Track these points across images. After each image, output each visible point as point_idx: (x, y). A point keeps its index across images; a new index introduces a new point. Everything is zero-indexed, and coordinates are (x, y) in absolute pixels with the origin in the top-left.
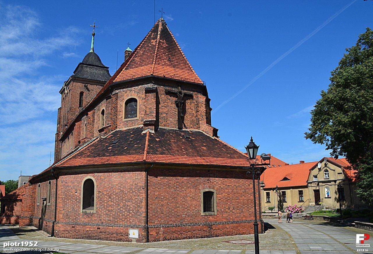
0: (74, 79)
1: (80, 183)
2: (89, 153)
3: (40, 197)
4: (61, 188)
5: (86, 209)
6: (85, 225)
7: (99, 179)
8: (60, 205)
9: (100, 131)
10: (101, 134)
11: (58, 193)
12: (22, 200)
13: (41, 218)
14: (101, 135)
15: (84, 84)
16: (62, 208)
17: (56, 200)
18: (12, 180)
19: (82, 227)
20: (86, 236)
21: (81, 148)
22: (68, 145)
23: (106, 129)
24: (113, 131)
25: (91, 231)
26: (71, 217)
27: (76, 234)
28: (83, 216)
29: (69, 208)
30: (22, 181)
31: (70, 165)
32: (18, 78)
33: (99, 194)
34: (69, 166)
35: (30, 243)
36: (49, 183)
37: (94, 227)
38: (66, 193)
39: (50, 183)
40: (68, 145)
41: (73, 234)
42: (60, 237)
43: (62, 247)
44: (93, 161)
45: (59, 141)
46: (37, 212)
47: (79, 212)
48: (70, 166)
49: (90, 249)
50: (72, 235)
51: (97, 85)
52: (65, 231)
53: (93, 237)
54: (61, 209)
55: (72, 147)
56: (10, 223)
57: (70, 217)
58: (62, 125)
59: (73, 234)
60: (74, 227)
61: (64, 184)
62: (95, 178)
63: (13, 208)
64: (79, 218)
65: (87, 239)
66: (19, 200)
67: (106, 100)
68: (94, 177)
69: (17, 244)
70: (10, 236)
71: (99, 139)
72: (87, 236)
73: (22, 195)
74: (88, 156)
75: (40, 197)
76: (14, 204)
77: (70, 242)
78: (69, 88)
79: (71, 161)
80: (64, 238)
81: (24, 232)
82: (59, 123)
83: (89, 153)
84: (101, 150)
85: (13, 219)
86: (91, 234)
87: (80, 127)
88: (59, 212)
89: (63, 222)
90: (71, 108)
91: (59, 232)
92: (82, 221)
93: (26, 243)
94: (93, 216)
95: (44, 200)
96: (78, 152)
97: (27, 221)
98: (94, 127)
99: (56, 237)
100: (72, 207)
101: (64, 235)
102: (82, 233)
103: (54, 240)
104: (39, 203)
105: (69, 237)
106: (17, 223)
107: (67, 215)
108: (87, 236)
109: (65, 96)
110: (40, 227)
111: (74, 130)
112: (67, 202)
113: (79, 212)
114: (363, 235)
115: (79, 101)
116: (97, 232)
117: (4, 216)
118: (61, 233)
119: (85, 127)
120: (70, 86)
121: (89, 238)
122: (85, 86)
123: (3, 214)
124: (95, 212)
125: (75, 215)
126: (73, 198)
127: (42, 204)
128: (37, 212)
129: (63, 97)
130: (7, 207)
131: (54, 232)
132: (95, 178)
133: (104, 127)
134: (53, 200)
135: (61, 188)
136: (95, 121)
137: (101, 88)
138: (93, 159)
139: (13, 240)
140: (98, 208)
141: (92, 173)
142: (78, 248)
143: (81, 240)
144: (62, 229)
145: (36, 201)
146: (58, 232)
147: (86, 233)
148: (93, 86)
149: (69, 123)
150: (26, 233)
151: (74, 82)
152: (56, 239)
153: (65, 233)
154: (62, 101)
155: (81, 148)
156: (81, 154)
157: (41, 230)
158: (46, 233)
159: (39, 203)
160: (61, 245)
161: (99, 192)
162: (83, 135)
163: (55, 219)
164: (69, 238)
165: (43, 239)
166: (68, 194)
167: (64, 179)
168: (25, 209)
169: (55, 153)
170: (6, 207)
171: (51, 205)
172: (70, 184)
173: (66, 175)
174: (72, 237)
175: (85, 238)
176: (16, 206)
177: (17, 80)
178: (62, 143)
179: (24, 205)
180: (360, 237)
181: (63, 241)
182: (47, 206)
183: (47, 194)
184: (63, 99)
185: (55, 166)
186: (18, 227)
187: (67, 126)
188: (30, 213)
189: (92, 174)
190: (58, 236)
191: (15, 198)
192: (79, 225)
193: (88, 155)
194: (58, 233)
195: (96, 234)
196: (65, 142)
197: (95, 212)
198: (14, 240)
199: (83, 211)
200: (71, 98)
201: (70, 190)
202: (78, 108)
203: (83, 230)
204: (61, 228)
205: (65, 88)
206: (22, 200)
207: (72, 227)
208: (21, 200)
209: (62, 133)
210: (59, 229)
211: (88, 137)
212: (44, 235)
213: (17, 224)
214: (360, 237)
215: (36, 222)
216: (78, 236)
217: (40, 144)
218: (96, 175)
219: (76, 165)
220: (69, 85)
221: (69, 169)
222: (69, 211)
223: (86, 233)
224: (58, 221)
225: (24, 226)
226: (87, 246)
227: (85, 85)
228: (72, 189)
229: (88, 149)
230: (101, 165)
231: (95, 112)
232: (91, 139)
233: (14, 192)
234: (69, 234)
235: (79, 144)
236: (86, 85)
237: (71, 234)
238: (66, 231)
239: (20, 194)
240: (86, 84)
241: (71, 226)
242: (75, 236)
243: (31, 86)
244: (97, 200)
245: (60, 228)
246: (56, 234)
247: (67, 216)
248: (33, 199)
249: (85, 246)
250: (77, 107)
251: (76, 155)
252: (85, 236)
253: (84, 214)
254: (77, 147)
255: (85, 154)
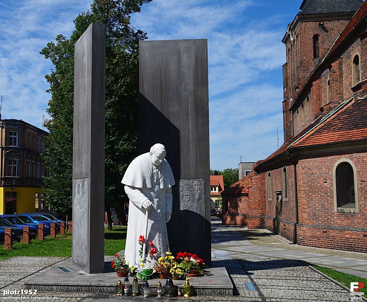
0: (302, 17)
1: (330, 169)
2: (341, 124)
3: (272, 190)
4: (303, 177)
5: (342, 206)
6: (342, 230)
7: (361, 161)
8: (303, 200)
9: (355, 89)
10: (357, 94)
11: (299, 184)
12: (248, 194)
13: (275, 218)
14: (357, 96)
15: (318, 23)
16: (305, 205)
17: (297, 194)
18: (230, 169)
19: (338, 232)
20: (346, 246)
21: (326, 119)
22: (302, 115)
23: (365, 85)
24: (326, 115)
25: (352, 238)
26: (320, 218)
27: (329, 242)
28: (338, 216)
29: (317, 205)
30: (243, 169)
31: (314, 144)
32: (219, 30)
33: (363, 184)
34: (312, 145)
35: (30, 292)
36: (284, 171)
37: (358, 233)
38: (310, 183)
39: (285, 170)
40: (302, 115)
41: (325, 242)
42: (306, 246)
43: (312, 259)
44: (348, 136)
45: (289, 111)
46: (270, 210)
47: (333, 211)
48: (313, 145)
49: (356, 265)
50: (324, 244)
51: (338, 20)
52: (313, 237)
53: (358, 248)
54: (305, 206)
55: (309, 118)
56: (235, 224)
57: (319, 217)
58: (290, 88)
59: (325, 242)
60: (326, 232)
61: (307, 171)
62: (354, 160)
63: (238, 204)
64: (332, 219)
65: (348, 251)
66: (244, 194)
67: (361, 40)
68: (352, 159)
69: (17, 292)
70: (239, 240)
71: (353, 102)
72: (348, 246)
73: (248, 188)
74: (340, 129)
75: (272, 190)
76: (239, 199)
77: (322, 252)
78: (295, 33)
79: (314, 138)
80: (312, 246)
81: (256, 236)
82: (286, 86)
83: (341, 124)
84: (360, 118)
85: (239, 219)
86: (353, 243)
87: (320, 88)
88: (302, 210)
89: (308, 225)
90: (301, 61)
91: (304, 238)
92: (338, 223)
93: (26, 291)
94: (355, 216)
95: (277, 194)
96: (323, 125)
97: (257, 222)
98: (343, 85)
99: (301, 245)
100: (320, 203)
101: (312, 242)
102: (339, 241)
103: (298, 249)
104: (271, 198)
105: (319, 245)
106: (244, 224)
107: (315, 215)
108: (348, 246)
109: (291, 46)
110: (275, 231)
111: (311, 93)
112: (313, 196)
113: (333, 211)
114: (357, 283)
115: (312, 49)
116: (363, 242)
117: (227, 215)
118: (307, 240)
119: (328, 87)
120: (297, 29)
121: (351, 249)
122: (320, 25)
123: (226, 212)
124: (357, 211)
125: (326, 215)
126: (322, 190)
127: (276, 200)
128: (270, 210)
129: (288, 48)
130: (230, 203)
131: (296, 238)
132: (354, 160)
133: (360, 82)
134: (291, 193)
135: (302, 176)
136: (344, 75)
137: (346, 23)
138: (348, 132)
139: (244, 246)
140: (362, 206)
141: (349, 154)
142: (336, 262)
143: (338, 250)
144: (308, 234)
145: (266, 196)
146: (302, 238)
147: (345, 242)
148: (332, 23)
149: (301, 84)
150: (259, 237)
151: (302, 22)
152: (300, 248)
153: (313, 241)
154: (288, 54)
155: (326, 119)
156: (328, 127)
157: (278, 234)
158: (285, 239)
159: (271, 198)
160: (312, 256)
161: (361, 181)
162: (326, 98)
163: (297, 220)
164: (320, 247)
165: (283, 247)
166: (313, 185)
167: (306, 164)
168: (254, 206)
169: (284, 128)
170: (229, 204)
171: (289, 201)
172: (315, 171)
173: (307, 159)
174: (325, 246)
175: (344, 248)
176: (241, 202)
177: (219, 33)
178: (293, 113)
179: (251, 200)
180: (355, 285)
181: (312, 251)
182: (283, 203)
183: (282, 186)
184: (288, 51)
185: (291, 146)
186: (246, 229)
187: (299, 88)
188: (260, 211)
189: (348, 155)
190: (303, 243)
191: (239, 192)
192: (334, 229)
193: (340, 127)
194: (303, 240)
195: (362, 244)
196: (298, 112)
197: (357, 211)
198: (246, 245)
199: (338, 210)
200: (300, 46)
201: (316, 179)
202: (313, 60)
203: (341, 237)
204: (307, 232)
205: (290, 34)
206: (248, 194)
207: (324, 232)
208: (247, 195)
209: (291, 99)
210: (304, 234)
211: (335, 100)
212: (284, 242)
213: (245, 225)
214: (354, 285)
215: (269, 223)
216: (332, 245)
217: (259, 117)
218: (355, 156)
219: (322, 143)
220: (296, 28)
221: (312, 150)
222: (317, 209)
223: (345, 242)
224: (302, 223)
225: (254, 228)
226: (350, 260)
227: (320, 24)
228: (318, 177)
229: (338, 118)
230: (362, 140)
231: (342, 62)
232: (340, 103)
233: (237, 183)
234: (319, 241)
235: (322, 112)
236: (322, 23)
237: (323, 242)
238: (315, 237)
239: (245, 186)
240: (322, 21)
241: (322, 231)
242: (328, 244)
243: (238, 39)
244: (360, 194)
245: (305, 232)
246: (300, 241)
247: (314, 216)
248: (263, 192)
249: (347, 260)
250: (310, 59)
251: (320, 129)
252: (344, 246)
253: (340, 214)
254: (317, 117)
255: (334, 127)
